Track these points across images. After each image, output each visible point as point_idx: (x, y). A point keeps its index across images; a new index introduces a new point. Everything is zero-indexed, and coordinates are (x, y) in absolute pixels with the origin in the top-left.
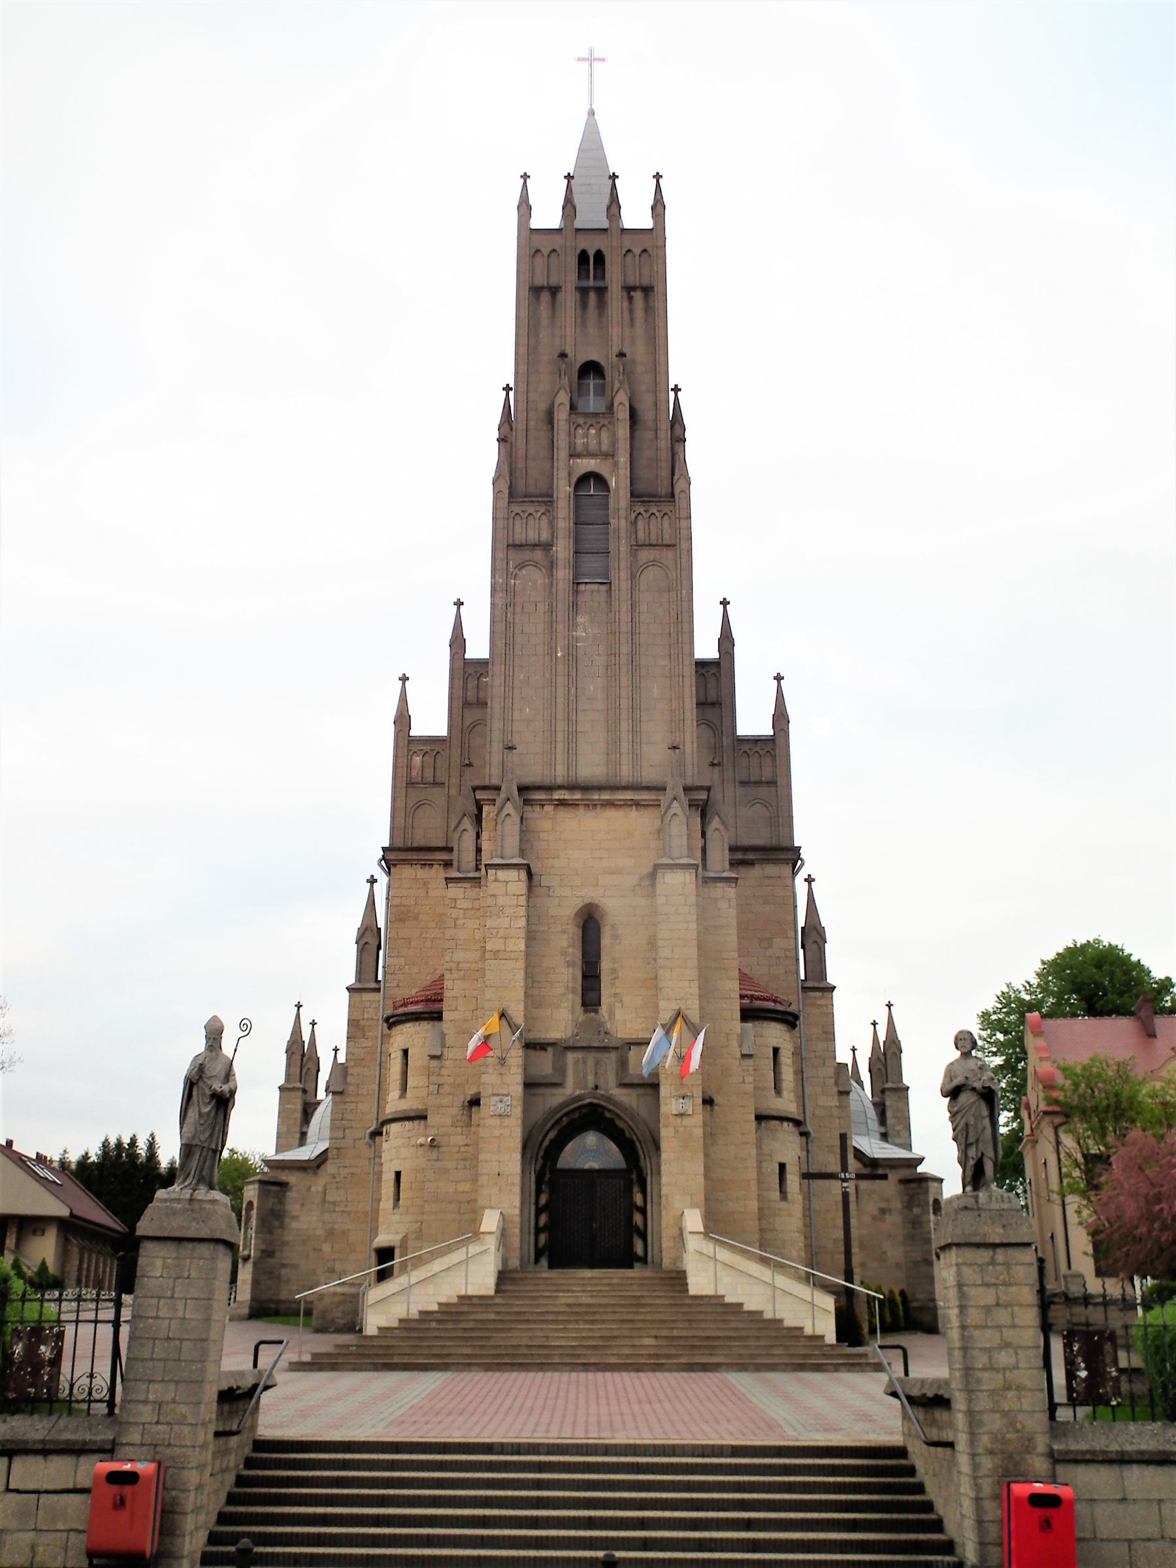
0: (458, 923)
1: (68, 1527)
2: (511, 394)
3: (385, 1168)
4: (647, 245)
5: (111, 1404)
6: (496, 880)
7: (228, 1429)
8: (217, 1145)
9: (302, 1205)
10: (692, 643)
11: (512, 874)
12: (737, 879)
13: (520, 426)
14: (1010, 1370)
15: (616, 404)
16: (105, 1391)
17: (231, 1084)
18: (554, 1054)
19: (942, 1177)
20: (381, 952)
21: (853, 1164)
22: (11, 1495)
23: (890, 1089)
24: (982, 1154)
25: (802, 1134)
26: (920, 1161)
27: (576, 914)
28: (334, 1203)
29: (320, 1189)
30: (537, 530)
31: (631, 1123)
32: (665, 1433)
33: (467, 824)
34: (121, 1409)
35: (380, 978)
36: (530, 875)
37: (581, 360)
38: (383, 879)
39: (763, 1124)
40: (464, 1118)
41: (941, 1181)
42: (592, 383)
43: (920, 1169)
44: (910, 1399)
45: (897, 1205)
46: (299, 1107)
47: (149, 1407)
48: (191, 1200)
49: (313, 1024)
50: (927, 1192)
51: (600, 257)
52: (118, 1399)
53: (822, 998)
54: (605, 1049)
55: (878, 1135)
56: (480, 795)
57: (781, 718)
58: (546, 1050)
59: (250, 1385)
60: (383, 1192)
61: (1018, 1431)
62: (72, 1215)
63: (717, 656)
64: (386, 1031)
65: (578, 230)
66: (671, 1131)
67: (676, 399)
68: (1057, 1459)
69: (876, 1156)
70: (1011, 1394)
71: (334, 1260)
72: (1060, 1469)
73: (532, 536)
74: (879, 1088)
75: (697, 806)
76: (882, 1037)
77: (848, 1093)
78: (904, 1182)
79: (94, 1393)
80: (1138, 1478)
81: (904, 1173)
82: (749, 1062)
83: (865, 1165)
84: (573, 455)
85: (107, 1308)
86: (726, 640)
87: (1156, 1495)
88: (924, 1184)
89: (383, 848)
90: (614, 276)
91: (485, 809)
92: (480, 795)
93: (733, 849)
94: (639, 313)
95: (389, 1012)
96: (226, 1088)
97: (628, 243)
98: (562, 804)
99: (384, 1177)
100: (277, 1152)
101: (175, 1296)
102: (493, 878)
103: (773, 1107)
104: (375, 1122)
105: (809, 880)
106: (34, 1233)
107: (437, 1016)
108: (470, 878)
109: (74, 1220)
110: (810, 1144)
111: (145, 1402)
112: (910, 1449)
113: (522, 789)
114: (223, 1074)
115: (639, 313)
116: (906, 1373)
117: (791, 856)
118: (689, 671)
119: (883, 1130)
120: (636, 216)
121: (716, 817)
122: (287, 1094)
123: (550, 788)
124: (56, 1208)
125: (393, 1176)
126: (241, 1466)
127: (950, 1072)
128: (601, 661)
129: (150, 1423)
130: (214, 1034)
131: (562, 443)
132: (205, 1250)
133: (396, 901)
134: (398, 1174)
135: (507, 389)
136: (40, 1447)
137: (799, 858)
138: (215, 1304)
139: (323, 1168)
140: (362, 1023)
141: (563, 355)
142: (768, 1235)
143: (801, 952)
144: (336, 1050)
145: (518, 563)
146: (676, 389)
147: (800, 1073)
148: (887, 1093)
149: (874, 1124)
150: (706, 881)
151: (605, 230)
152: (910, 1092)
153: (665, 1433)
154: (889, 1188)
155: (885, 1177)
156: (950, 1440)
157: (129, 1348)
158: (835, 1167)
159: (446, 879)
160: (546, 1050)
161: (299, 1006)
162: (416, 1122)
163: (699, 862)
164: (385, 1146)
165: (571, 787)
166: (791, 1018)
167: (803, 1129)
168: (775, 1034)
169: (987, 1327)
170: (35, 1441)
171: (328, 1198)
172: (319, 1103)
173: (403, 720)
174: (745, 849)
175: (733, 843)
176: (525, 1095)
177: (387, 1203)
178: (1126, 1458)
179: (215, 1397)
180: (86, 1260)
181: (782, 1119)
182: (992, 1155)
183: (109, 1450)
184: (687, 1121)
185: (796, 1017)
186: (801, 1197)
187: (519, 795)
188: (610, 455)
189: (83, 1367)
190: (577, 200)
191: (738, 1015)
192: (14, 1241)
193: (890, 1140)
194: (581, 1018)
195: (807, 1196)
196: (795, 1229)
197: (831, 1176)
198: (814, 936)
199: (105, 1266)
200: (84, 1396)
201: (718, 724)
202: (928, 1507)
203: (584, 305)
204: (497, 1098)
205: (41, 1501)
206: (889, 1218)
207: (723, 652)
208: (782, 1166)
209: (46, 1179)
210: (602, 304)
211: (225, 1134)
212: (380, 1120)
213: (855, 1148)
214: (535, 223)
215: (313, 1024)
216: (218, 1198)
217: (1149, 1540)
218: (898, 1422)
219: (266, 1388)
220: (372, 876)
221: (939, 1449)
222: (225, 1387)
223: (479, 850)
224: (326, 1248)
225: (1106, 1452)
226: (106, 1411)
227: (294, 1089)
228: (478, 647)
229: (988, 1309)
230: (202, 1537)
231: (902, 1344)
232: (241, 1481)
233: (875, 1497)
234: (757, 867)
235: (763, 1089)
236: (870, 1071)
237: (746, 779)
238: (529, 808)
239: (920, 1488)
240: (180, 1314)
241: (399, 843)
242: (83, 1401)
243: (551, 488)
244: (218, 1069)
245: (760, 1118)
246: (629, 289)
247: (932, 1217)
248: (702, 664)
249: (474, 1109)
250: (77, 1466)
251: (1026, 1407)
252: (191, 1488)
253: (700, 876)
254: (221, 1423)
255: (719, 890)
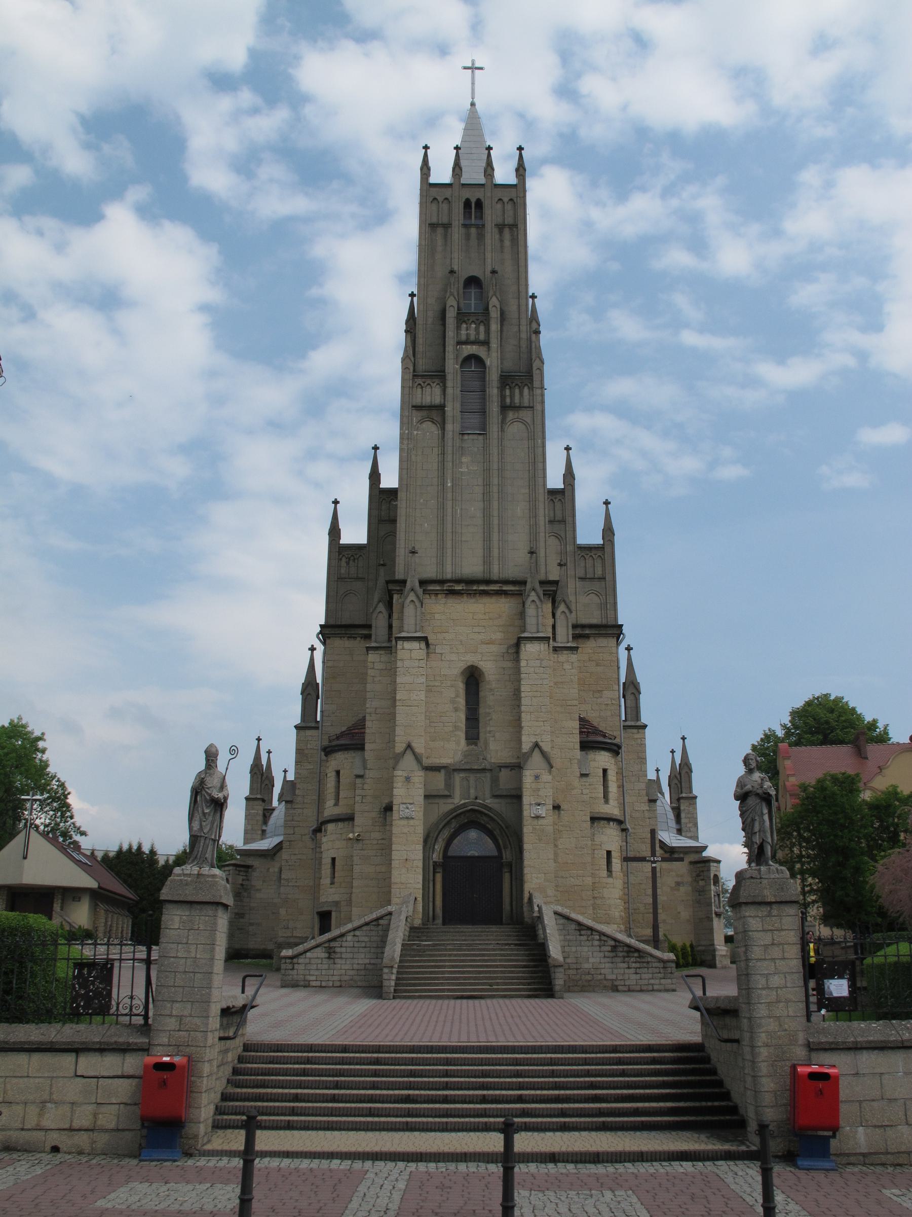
0: (375, 679)
1: (119, 1102)
2: (415, 299)
3: (324, 855)
4: (513, 195)
5: (146, 1017)
6: (403, 649)
7: (226, 1035)
8: (215, 836)
9: (264, 881)
10: (545, 477)
11: (415, 645)
12: (578, 648)
13: (419, 322)
14: (781, 988)
15: (490, 306)
16: (142, 1007)
17: (225, 793)
18: (445, 775)
19: (720, 859)
20: (319, 701)
21: (659, 851)
22: (79, 1079)
23: (683, 798)
24: (763, 840)
25: (623, 830)
26: (704, 848)
27: (462, 673)
28: (287, 880)
29: (277, 870)
30: (432, 395)
31: (500, 823)
32: (534, 1037)
33: (381, 607)
34: (153, 1020)
35: (318, 719)
36: (428, 645)
37: (464, 275)
38: (320, 648)
39: (596, 824)
40: (381, 819)
41: (719, 862)
42: (473, 291)
43: (704, 854)
44: (707, 1010)
45: (688, 879)
46: (261, 812)
47: (173, 1020)
48: (199, 875)
49: (269, 752)
50: (709, 870)
51: (479, 204)
52: (151, 1014)
53: (638, 732)
54: (484, 770)
55: (675, 831)
56: (391, 587)
57: (608, 531)
58: (440, 771)
59: (241, 1005)
60: (323, 872)
61: (786, 1030)
62: (100, 887)
63: (562, 486)
64: (324, 757)
65: (463, 185)
66: (530, 828)
67: (534, 304)
68: (812, 1048)
69: (674, 845)
70: (781, 1005)
71: (288, 920)
72: (814, 1055)
73: (427, 400)
74: (675, 797)
75: (549, 595)
76: (678, 761)
77: (655, 801)
78: (692, 863)
79: (134, 1010)
80: (867, 1060)
81: (693, 857)
82: (584, 779)
83: (666, 852)
84: (460, 343)
85: (141, 951)
86: (569, 475)
87: (878, 1070)
88: (707, 864)
89: (321, 626)
90: (491, 215)
91: (395, 597)
92: (391, 587)
93: (575, 626)
94: (507, 243)
95: (326, 743)
96: (221, 795)
97: (499, 194)
98: (451, 593)
99: (324, 861)
100: (245, 843)
101: (189, 942)
102: (401, 647)
103: (602, 811)
104: (316, 822)
105: (629, 649)
106: (74, 899)
107: (361, 747)
108: (384, 647)
109: (102, 891)
110: (628, 837)
111: (171, 1016)
112: (707, 1045)
113: (422, 583)
114: (219, 785)
115: (507, 243)
116: (704, 993)
117: (614, 631)
118: (542, 497)
119: (678, 827)
120: (504, 174)
121: (563, 603)
122: (251, 803)
123: (442, 582)
124: (88, 882)
125: (330, 861)
126: (236, 1061)
127: (740, 783)
128: (479, 490)
129: (174, 1030)
130: (211, 756)
131: (450, 333)
132: (209, 911)
133: (330, 664)
134: (334, 859)
135: (412, 295)
136: (98, 1046)
137: (621, 633)
138: (217, 948)
139: (278, 855)
140: (306, 751)
141: (452, 272)
142: (598, 902)
143: (622, 700)
144: (285, 771)
145: (420, 419)
146: (533, 297)
147: (621, 787)
148: (682, 801)
149: (672, 823)
150: (556, 649)
151: (483, 185)
152: (698, 800)
153: (534, 1037)
154: (681, 868)
155: (682, 860)
156: (736, 1038)
157: (158, 978)
158: (647, 853)
159: (367, 648)
160: (440, 771)
161: (259, 739)
162: (346, 823)
163: (550, 635)
164: (324, 840)
165: (458, 581)
166: (615, 748)
167: (623, 826)
168: (603, 759)
169: (765, 959)
170: (94, 1043)
171: (283, 876)
172: (273, 810)
173: (334, 531)
174: (583, 626)
175: (575, 622)
176: (425, 804)
177: (326, 881)
178: (859, 1046)
179: (219, 1012)
180: (110, 919)
181: (609, 819)
182: (769, 840)
183: (145, 1050)
184: (541, 822)
185: (619, 747)
186: (622, 874)
187: (420, 586)
188: (486, 343)
189: (125, 992)
190: (463, 163)
191: (578, 746)
192: (59, 905)
193: (683, 834)
194: (466, 748)
195: (627, 874)
196: (617, 896)
197: (643, 859)
198: (632, 688)
199: (123, 923)
200: (127, 1011)
201: (564, 538)
202: (720, 1084)
203: (468, 237)
204: (404, 806)
205: (100, 1083)
206: (682, 889)
207: (566, 484)
208: (609, 853)
209: (81, 861)
210: (481, 237)
211: (220, 828)
212: (320, 821)
213: (660, 840)
214: (433, 180)
215: (269, 752)
216: (218, 873)
217: (873, 1100)
218: (698, 1027)
219: (253, 1007)
220: (313, 646)
221: (729, 1044)
222: (225, 1006)
223: (390, 627)
224: (283, 911)
225: (845, 1043)
226: (142, 1022)
227: (256, 799)
228: (390, 480)
229: (766, 947)
230: (212, 1108)
231: (701, 974)
232: (236, 1072)
233: (683, 1078)
234: (592, 639)
235: (595, 798)
236: (669, 785)
237: (583, 576)
238: (428, 596)
239: (714, 1072)
240: (193, 955)
241: (332, 622)
242: (126, 1015)
243: (444, 366)
244: (213, 782)
245: (593, 819)
246: (501, 227)
247: (713, 887)
248: (553, 492)
249: (388, 814)
250: (124, 1059)
251: (791, 1013)
252: (205, 1075)
253: (551, 646)
254: (222, 1032)
255: (564, 657)
